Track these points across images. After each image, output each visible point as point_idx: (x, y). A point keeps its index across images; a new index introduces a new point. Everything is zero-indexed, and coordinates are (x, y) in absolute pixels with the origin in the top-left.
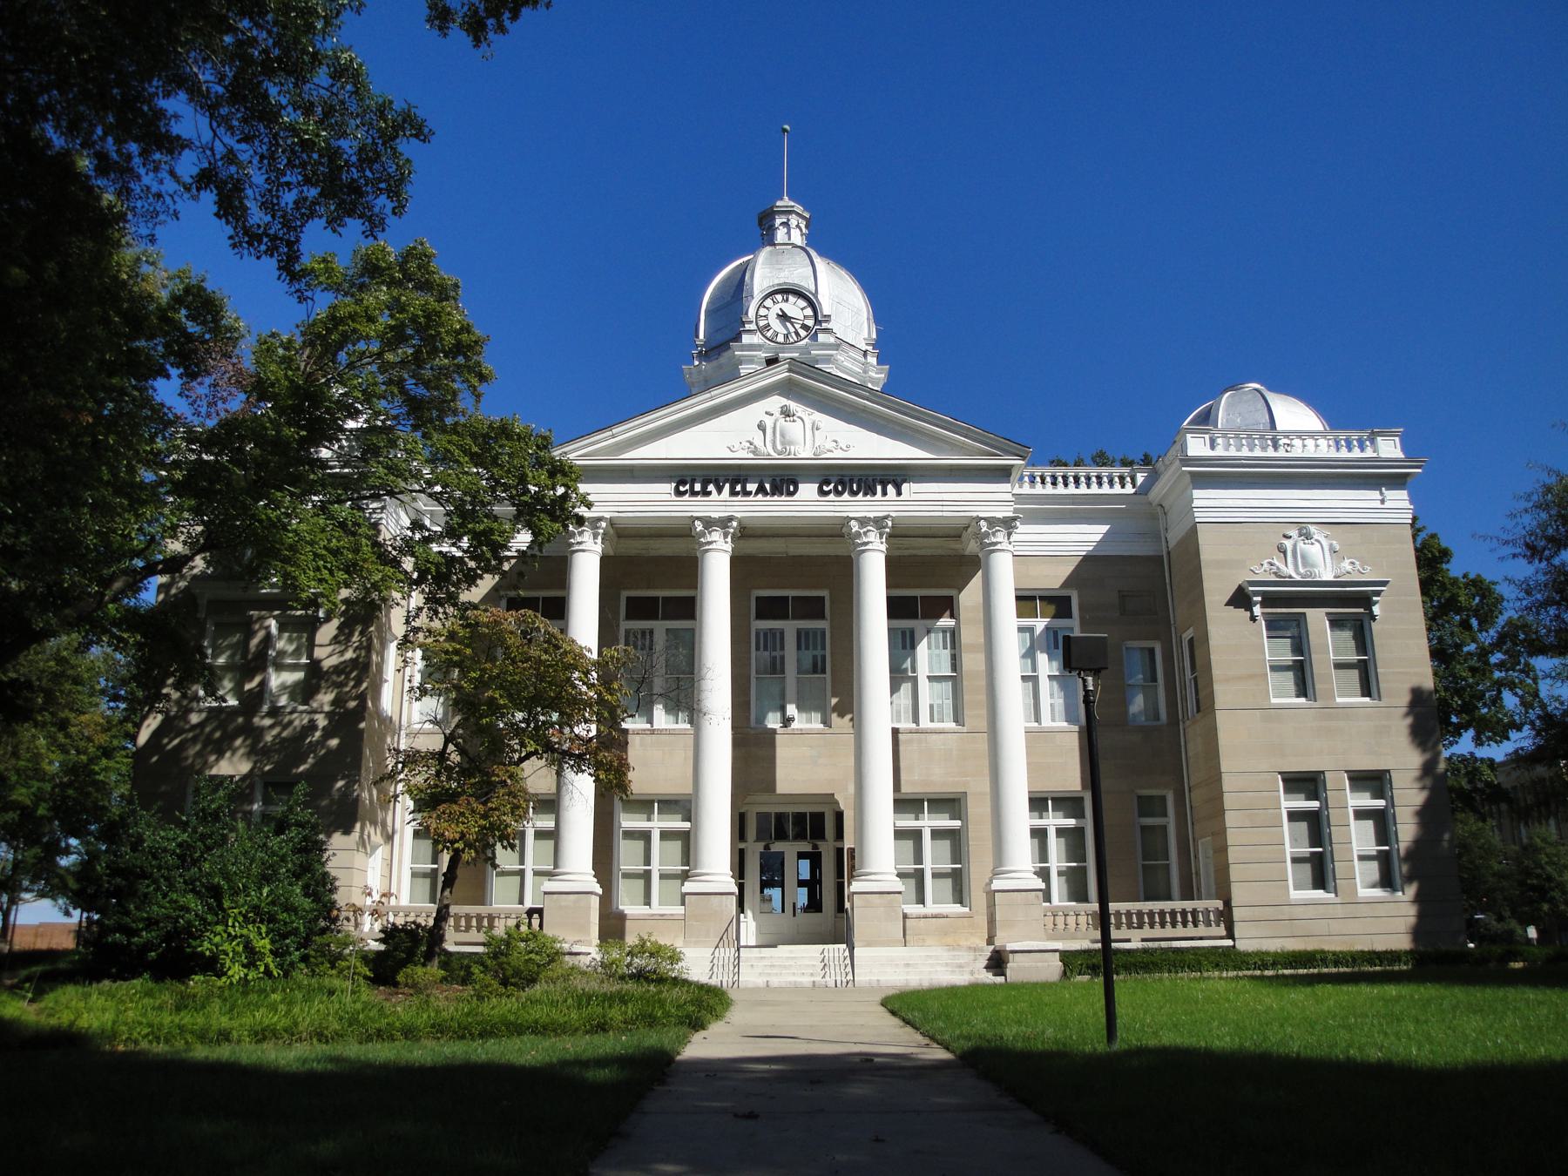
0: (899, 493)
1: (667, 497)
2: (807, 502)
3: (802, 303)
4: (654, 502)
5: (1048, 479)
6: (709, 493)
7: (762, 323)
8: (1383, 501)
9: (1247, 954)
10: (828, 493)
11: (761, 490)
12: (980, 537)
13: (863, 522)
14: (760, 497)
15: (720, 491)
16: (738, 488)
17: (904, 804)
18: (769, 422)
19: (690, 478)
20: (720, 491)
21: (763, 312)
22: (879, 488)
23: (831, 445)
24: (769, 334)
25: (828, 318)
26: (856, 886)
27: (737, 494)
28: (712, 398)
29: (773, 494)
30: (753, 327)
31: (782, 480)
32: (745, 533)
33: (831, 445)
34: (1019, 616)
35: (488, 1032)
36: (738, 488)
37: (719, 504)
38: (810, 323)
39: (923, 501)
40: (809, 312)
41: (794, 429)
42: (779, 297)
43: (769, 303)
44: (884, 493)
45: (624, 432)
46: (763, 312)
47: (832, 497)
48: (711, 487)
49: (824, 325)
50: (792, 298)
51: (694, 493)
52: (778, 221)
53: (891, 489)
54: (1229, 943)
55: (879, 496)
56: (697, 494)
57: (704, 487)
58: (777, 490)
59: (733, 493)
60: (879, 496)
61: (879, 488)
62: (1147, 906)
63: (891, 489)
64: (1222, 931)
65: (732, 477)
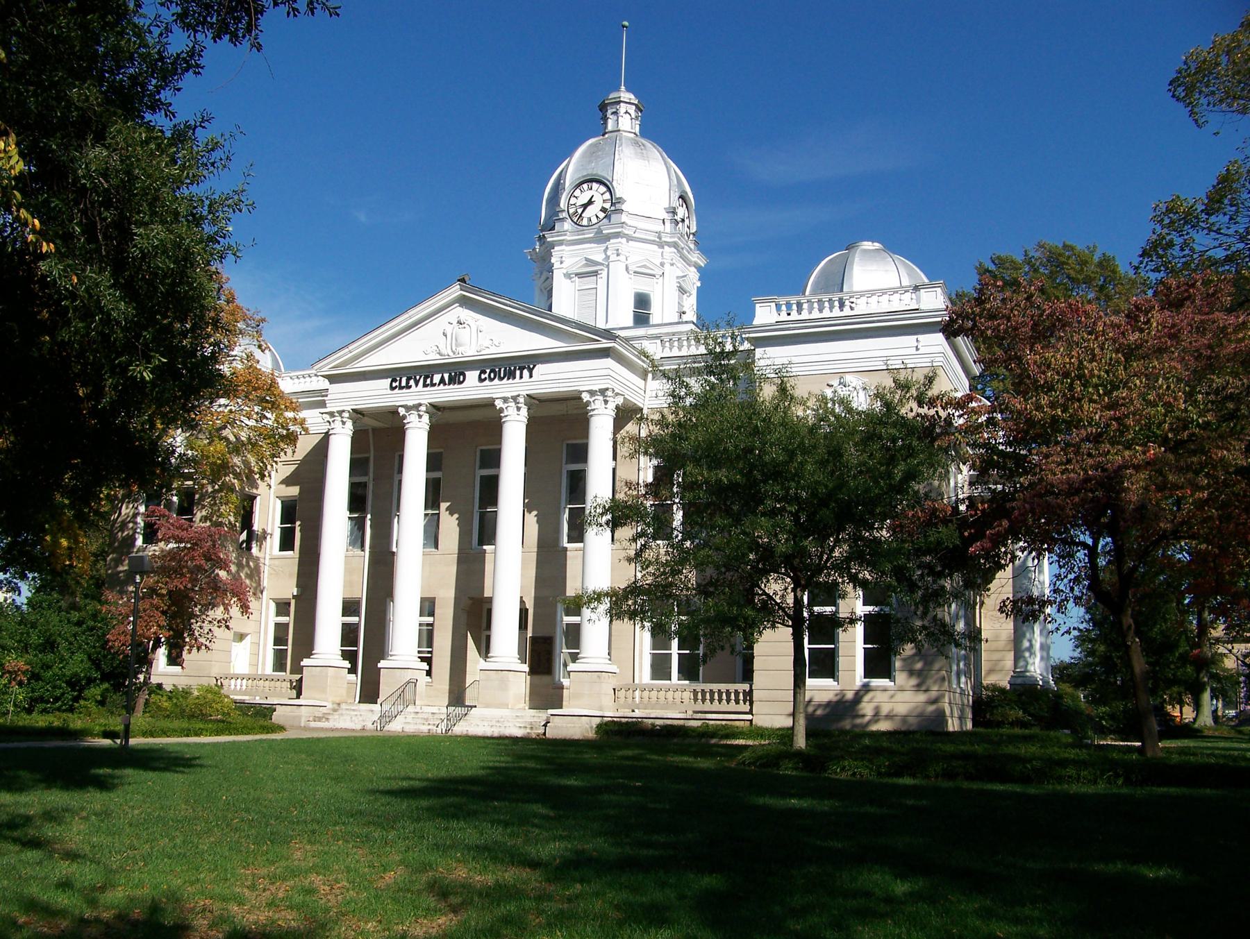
0: (521, 377)
1: (385, 392)
2: (472, 388)
3: (603, 189)
4: (376, 394)
8: (917, 349)
9: (761, 728)
13: (505, 400)
15: (417, 383)
16: (428, 381)
19: (401, 376)
20: (417, 383)
21: (573, 201)
22: (518, 372)
23: (488, 343)
26: (382, 664)
28: (410, 317)
30: (565, 215)
31: (455, 373)
32: (435, 409)
33: (488, 343)
35: (165, 733)
36: (428, 381)
37: (421, 395)
38: (607, 206)
39: (550, 379)
40: (607, 196)
41: (464, 334)
43: (577, 193)
44: (521, 377)
45: (356, 348)
46: (573, 201)
48: (412, 382)
50: (595, 185)
51: (401, 388)
52: (609, 112)
53: (526, 372)
54: (749, 717)
57: (408, 382)
58: (452, 380)
59: (425, 385)
61: (518, 372)
62: (723, 687)
63: (526, 372)
64: (747, 708)
65: (422, 374)
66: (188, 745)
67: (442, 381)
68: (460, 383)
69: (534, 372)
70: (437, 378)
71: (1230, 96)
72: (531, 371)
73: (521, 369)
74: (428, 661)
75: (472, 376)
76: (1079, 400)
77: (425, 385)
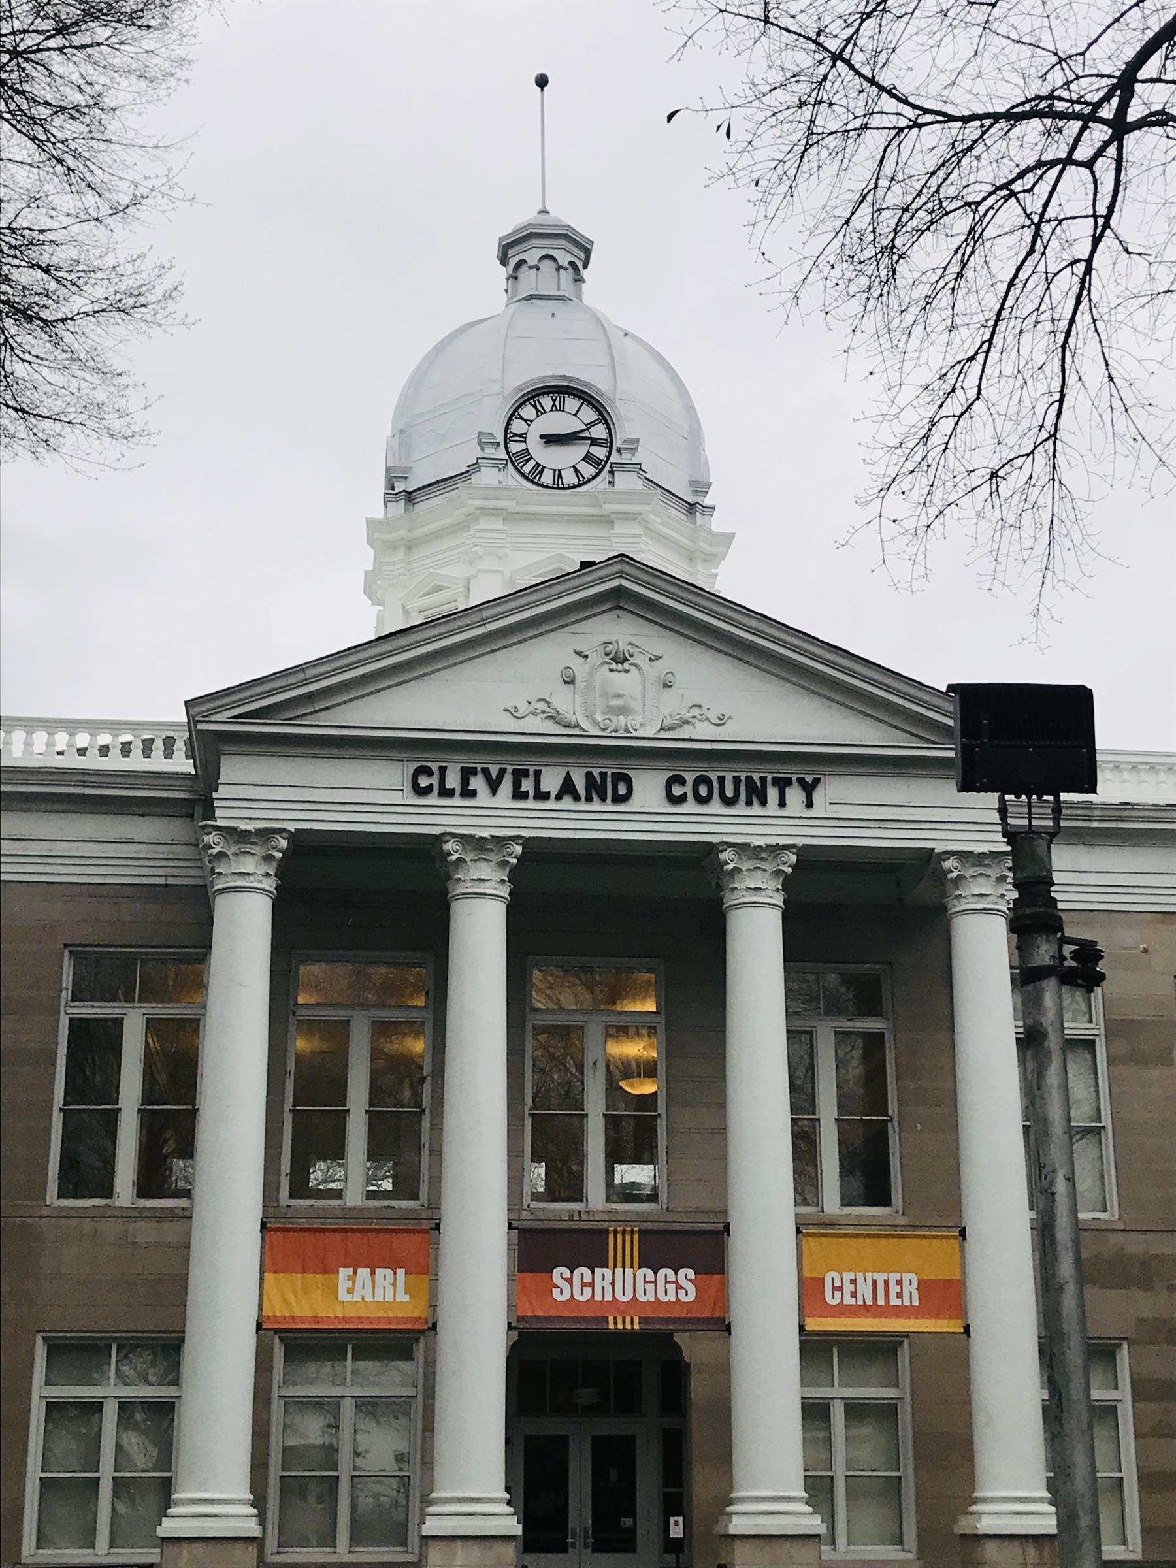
0: (782, 804)
1: (396, 798)
2: (648, 814)
5: (159, 745)
6: (473, 794)
7: (515, 447)
10: (682, 799)
11: (567, 789)
12: (941, 876)
14: (567, 803)
17: (815, 1349)
18: (580, 669)
24: (527, 469)
25: (633, 446)
27: (524, 796)
29: (589, 799)
31: (606, 770)
34: (804, 1383)
36: (527, 785)
37: (496, 814)
41: (626, 683)
42: (546, 402)
44: (782, 804)
47: (690, 806)
49: (626, 458)
51: (446, 793)
53: (795, 795)
55: (772, 807)
56: (450, 793)
57: (465, 782)
58: (596, 788)
59: (519, 795)
60: (772, 807)
63: (795, 795)
65: (509, 762)
66: (543, 1210)
67: (567, 789)
68: (618, 799)
69: (817, 796)
70: (551, 781)
71: (826, 1014)
72: (809, 789)
73: (782, 784)
74: (357, 1454)
75: (648, 789)
76: (941, 202)
77: (519, 795)
